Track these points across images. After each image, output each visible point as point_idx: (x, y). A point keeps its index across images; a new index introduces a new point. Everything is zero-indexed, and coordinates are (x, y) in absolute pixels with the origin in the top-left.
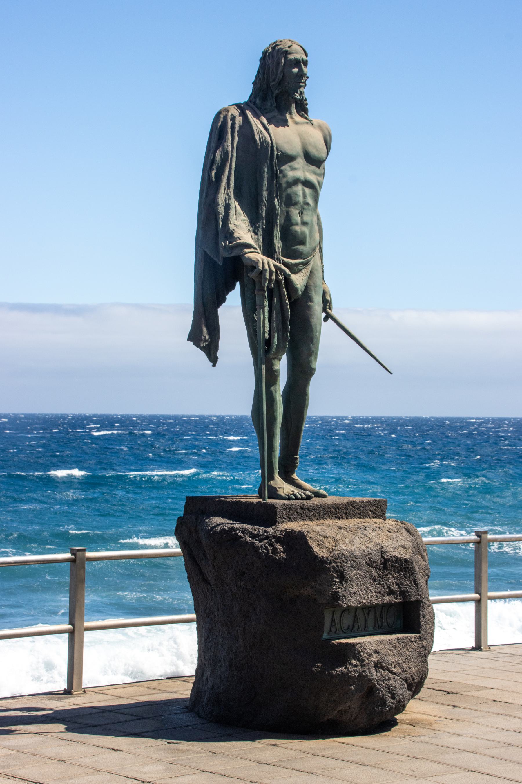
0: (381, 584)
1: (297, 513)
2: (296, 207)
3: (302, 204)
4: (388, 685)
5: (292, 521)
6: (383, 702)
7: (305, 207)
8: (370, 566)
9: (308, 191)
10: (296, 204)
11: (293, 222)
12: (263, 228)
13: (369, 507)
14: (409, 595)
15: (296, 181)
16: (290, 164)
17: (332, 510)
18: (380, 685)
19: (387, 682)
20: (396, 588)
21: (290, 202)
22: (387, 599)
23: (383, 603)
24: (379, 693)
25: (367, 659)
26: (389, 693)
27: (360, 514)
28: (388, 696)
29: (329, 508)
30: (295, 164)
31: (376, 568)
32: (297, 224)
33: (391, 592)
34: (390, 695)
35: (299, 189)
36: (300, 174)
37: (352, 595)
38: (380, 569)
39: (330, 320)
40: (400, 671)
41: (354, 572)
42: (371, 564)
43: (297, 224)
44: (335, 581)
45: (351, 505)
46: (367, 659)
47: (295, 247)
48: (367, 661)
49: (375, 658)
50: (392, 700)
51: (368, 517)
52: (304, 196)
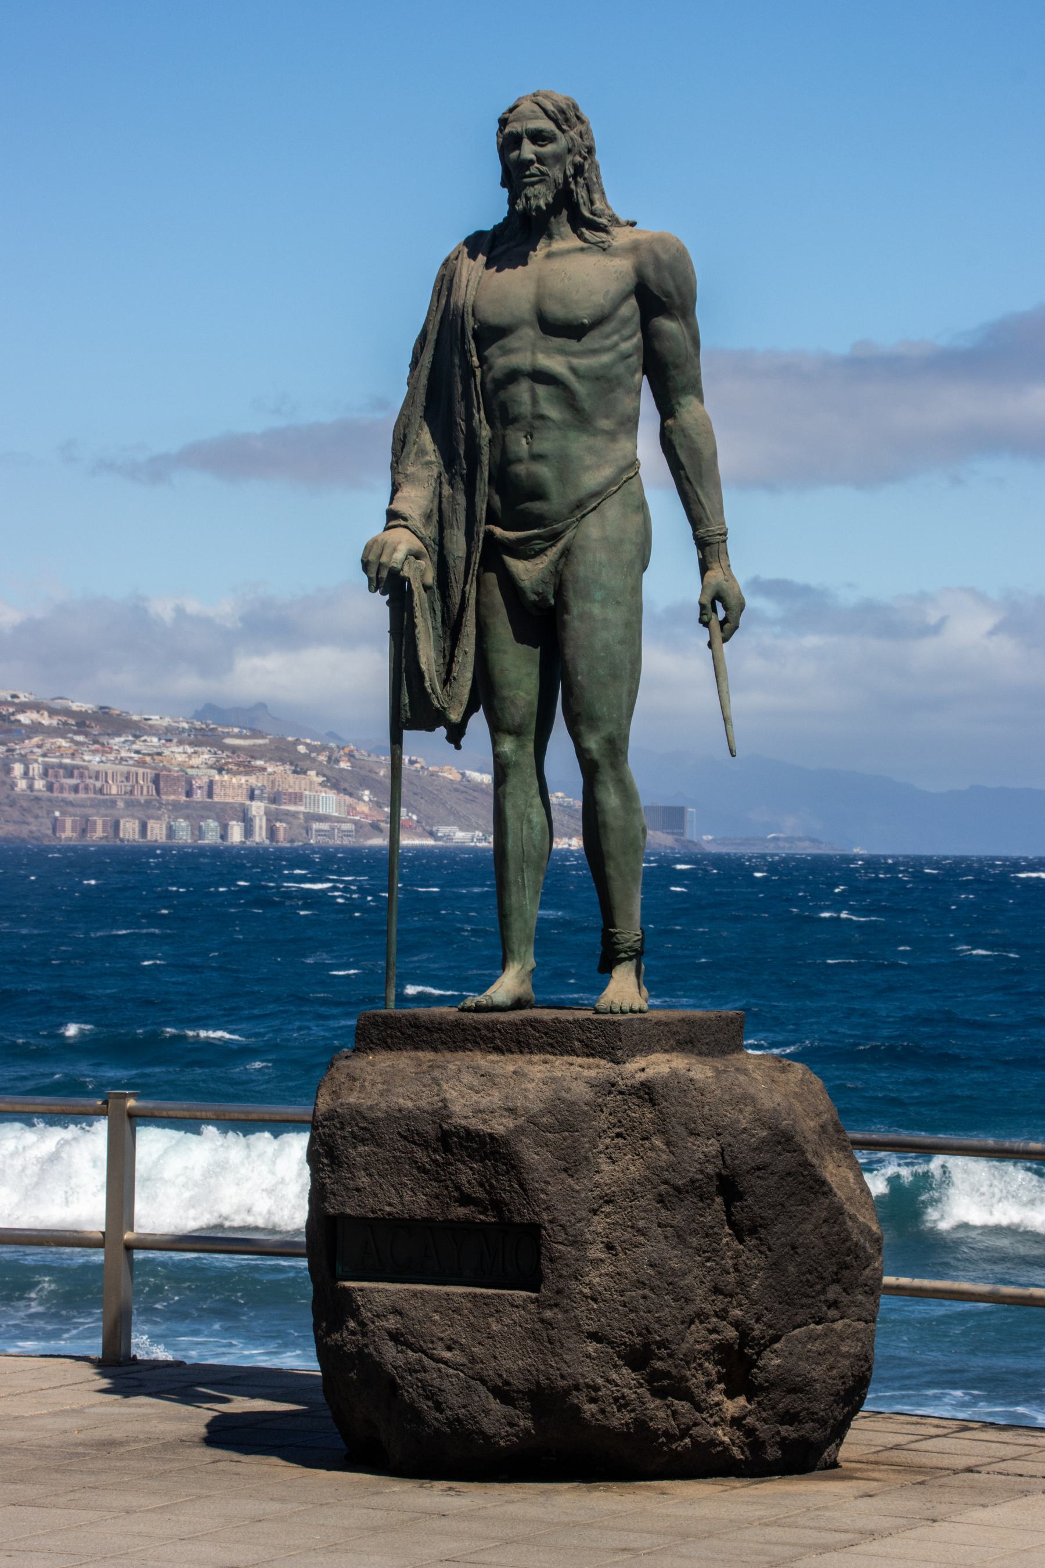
0: (441, 1181)
1: (402, 1034)
2: (517, 425)
3: (529, 419)
4: (421, 1381)
5: (391, 1050)
6: (418, 1415)
7: (537, 423)
8: (409, 1142)
9: (541, 390)
10: (515, 420)
11: (512, 456)
12: (462, 476)
13: (576, 1032)
14: (509, 1210)
15: (513, 376)
16: (500, 343)
17: (484, 1032)
18: (402, 1378)
19: (419, 1376)
20: (480, 1193)
21: (502, 417)
22: (461, 1212)
23: (446, 1221)
24: (402, 1395)
25: (373, 1322)
26: (427, 1398)
27: (552, 1046)
28: (425, 1405)
29: (476, 1028)
30: (511, 341)
31: (425, 1145)
32: (519, 460)
33: (465, 1200)
34: (430, 1404)
35: (522, 391)
36: (522, 360)
37: (350, 1194)
38: (435, 1151)
40: (465, 1360)
41: (361, 1149)
42: (413, 1137)
43: (519, 460)
44: (323, 1163)
45: (531, 1026)
46: (373, 1322)
47: (522, 506)
48: (373, 1327)
49: (392, 1322)
50: (438, 1415)
51: (574, 1052)
52: (535, 401)
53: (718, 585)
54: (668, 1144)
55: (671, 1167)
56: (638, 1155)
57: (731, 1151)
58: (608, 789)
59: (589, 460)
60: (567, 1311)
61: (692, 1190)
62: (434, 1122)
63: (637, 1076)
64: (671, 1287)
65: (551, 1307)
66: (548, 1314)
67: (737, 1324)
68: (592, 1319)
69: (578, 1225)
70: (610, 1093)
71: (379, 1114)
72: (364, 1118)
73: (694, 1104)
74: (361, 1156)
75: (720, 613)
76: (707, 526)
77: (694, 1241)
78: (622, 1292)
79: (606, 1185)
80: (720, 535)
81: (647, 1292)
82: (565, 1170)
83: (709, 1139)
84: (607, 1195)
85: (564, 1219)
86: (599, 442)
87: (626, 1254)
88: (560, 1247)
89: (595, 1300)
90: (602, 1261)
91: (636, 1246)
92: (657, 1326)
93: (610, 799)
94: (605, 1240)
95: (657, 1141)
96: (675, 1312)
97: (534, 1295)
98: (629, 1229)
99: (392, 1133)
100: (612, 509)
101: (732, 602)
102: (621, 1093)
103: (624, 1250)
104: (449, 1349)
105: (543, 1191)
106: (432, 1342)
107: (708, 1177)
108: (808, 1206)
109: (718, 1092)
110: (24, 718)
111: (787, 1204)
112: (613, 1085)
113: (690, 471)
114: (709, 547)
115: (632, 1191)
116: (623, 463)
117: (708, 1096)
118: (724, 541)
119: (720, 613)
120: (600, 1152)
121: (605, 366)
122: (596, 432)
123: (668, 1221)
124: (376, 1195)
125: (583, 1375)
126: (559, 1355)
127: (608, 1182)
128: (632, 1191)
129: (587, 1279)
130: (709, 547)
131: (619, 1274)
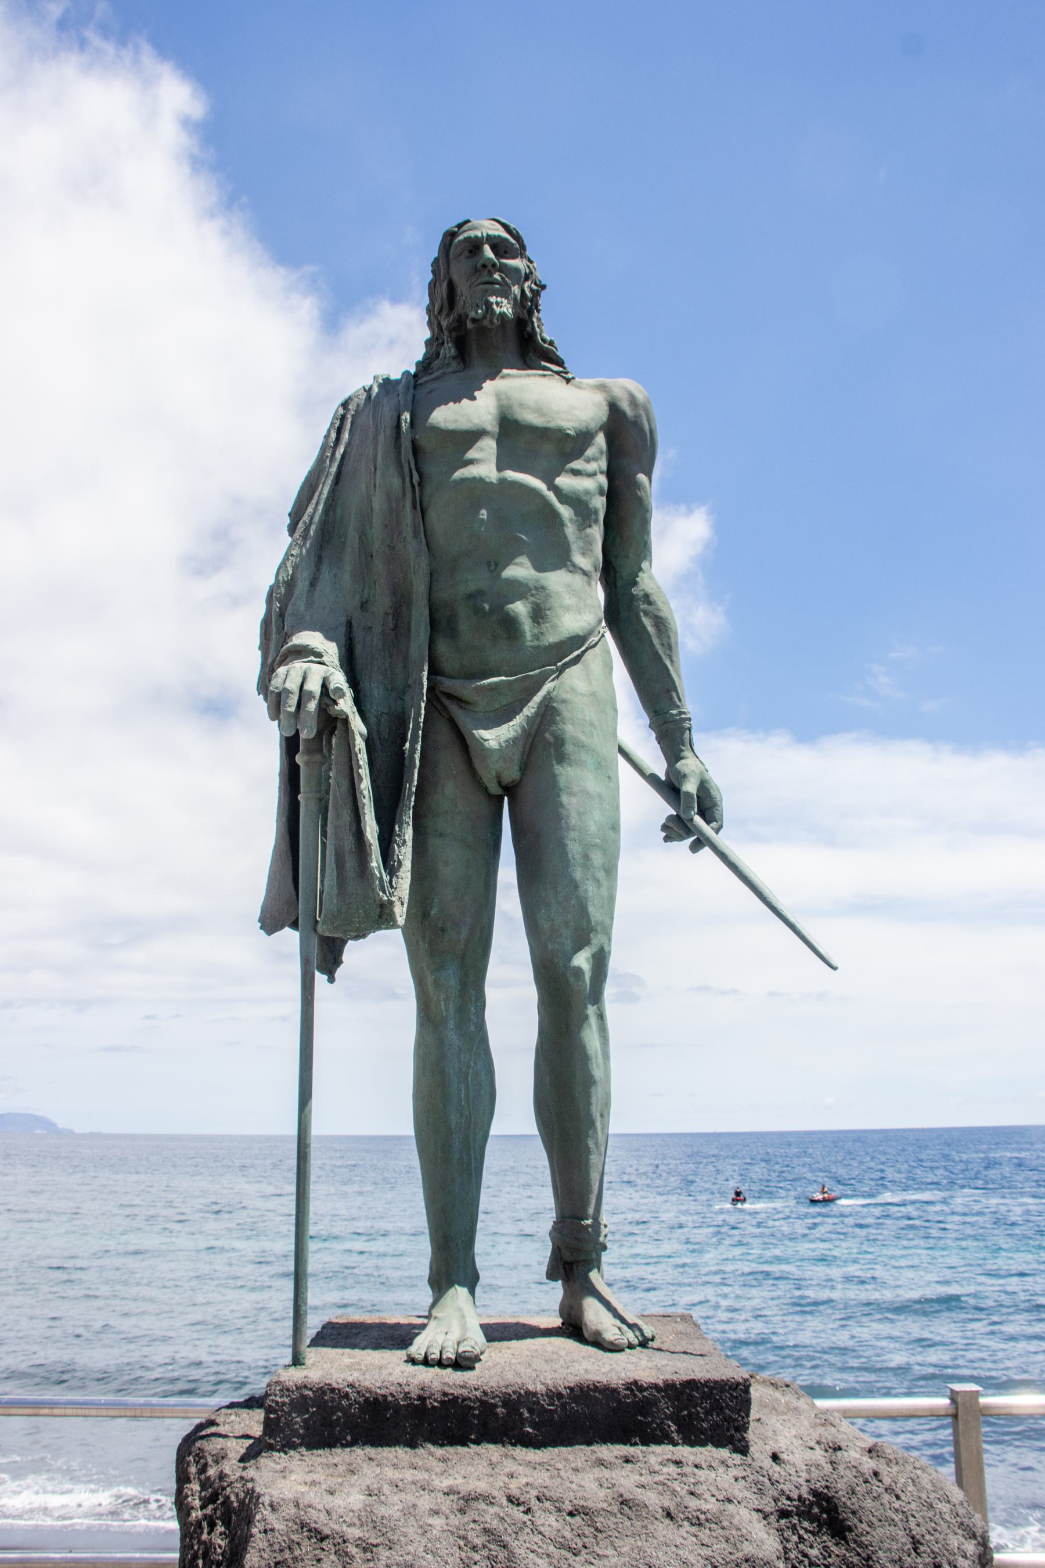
39: (707, 849)
59: (568, 600)
122: (575, 569)
130: (672, 733)
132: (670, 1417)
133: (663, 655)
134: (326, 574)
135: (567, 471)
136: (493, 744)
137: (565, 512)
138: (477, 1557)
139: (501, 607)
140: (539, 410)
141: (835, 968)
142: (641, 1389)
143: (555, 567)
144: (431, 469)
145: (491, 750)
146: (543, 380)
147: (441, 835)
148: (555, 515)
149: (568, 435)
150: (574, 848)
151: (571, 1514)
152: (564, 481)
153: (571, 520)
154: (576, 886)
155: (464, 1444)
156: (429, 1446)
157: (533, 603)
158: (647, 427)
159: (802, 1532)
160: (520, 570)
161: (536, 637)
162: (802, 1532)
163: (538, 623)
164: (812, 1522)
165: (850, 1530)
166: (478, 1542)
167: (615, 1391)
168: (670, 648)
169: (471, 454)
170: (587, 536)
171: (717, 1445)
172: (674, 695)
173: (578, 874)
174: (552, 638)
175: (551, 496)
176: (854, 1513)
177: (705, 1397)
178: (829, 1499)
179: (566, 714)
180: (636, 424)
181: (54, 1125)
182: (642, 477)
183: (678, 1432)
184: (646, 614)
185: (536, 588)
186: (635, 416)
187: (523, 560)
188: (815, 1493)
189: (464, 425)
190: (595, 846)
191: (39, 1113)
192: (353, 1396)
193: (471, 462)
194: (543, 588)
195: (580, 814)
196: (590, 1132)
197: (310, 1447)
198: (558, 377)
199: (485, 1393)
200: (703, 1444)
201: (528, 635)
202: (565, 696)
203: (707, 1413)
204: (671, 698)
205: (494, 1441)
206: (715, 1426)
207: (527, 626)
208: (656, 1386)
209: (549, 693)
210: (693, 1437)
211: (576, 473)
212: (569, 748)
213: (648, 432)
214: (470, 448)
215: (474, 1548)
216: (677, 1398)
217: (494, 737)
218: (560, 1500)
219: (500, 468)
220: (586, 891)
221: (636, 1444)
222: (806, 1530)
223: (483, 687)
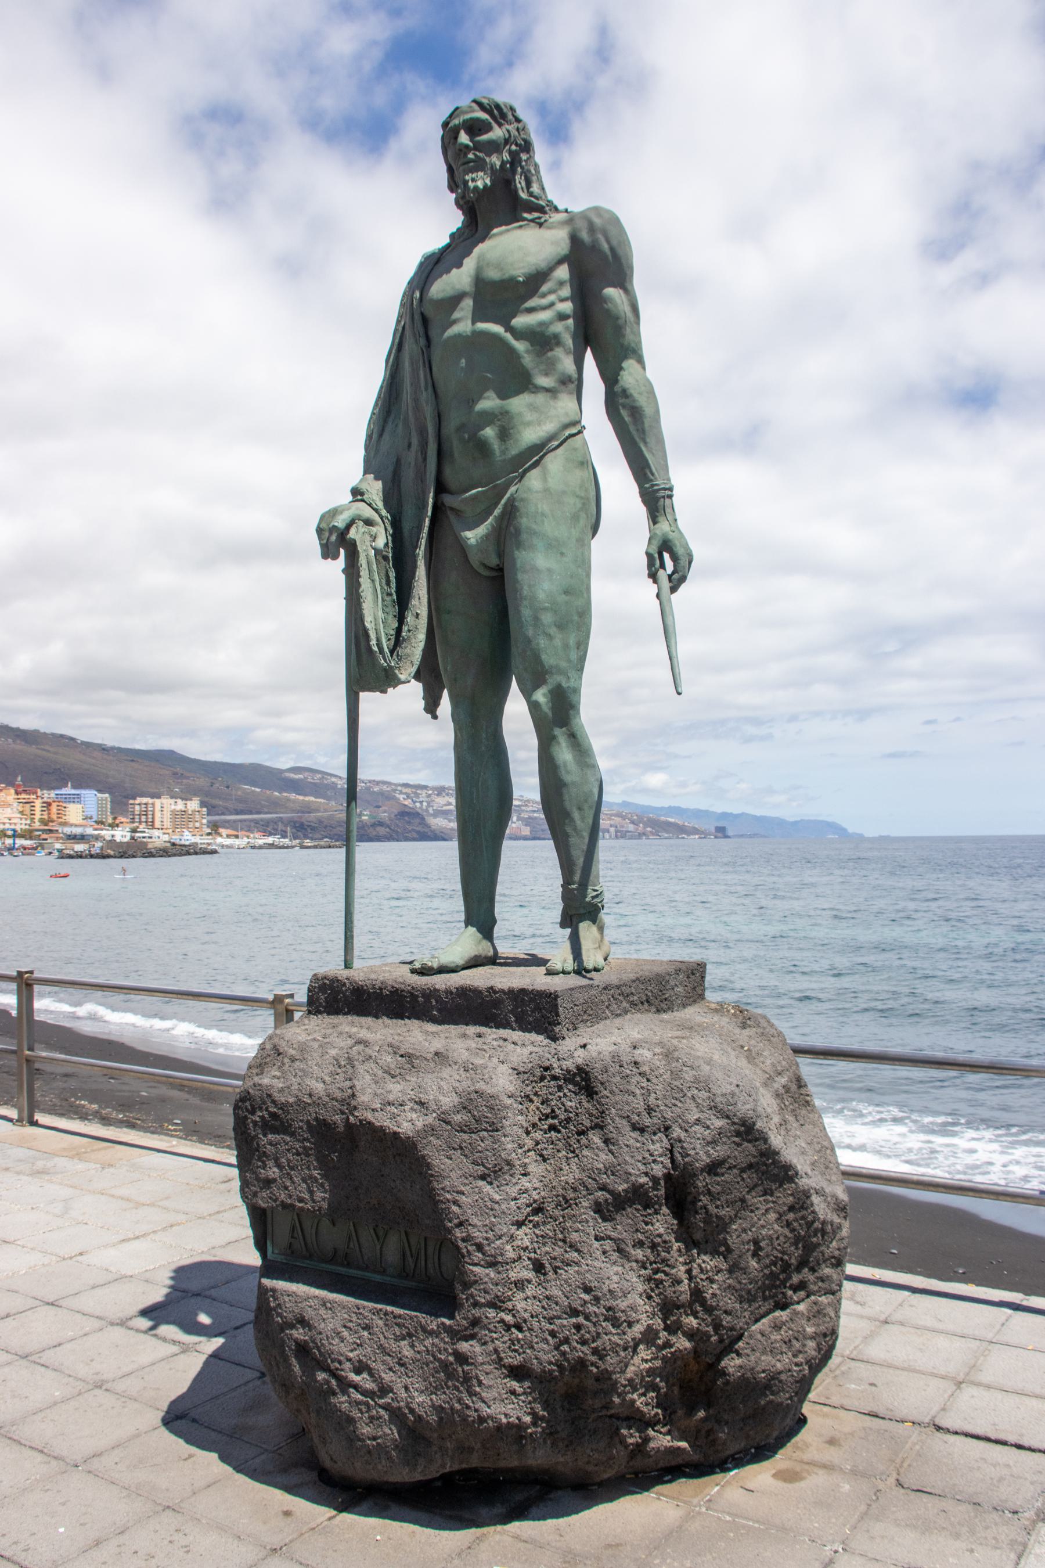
42: (322, 1130)
53: (664, 535)
54: (607, 1141)
55: (611, 1170)
56: (573, 1152)
57: (682, 1147)
58: (559, 743)
59: (529, 416)
60: (485, 1343)
61: (637, 1197)
62: (343, 1113)
63: (576, 1054)
64: (610, 1313)
65: (466, 1338)
66: (464, 1346)
67: (691, 1335)
68: (516, 1351)
69: (498, 1242)
70: (542, 1078)
71: (291, 1100)
72: (274, 1102)
73: (638, 1092)
74: (271, 1144)
75: (668, 562)
76: (652, 481)
77: (639, 1254)
78: (550, 1320)
79: (535, 1189)
80: (665, 489)
81: (581, 1319)
82: (483, 1177)
83: (655, 1134)
84: (535, 1201)
85: (478, 1235)
86: (540, 398)
87: (556, 1273)
88: (476, 1269)
89: (519, 1328)
90: (529, 1281)
91: (568, 1265)
92: (593, 1358)
93: (564, 754)
94: (532, 1255)
95: (596, 1138)
96: (615, 1339)
97: (447, 1322)
98: (560, 1243)
99: (302, 1121)
100: (555, 463)
101: (680, 551)
102: (555, 1078)
103: (555, 1270)
104: (358, 1372)
105: (456, 1203)
106: (340, 1362)
107: (655, 1180)
108: (772, 1195)
109: (667, 1076)
110: (516, 713)
111: (748, 1197)
112: (546, 1069)
113: (633, 423)
114: (656, 500)
115: (564, 1197)
116: (566, 420)
117: (654, 1081)
118: (670, 497)
119: (668, 562)
120: (529, 1150)
121: (542, 324)
122: (537, 389)
123: (608, 1233)
124: (286, 1188)
125: (506, 1415)
126: (476, 1394)
127: (537, 1185)
128: (564, 1197)
129: (509, 1305)
130: (656, 500)
131: (548, 1298)
132: (511, 1012)
133: (638, 439)
134: (389, 427)
135: (522, 312)
136: (473, 541)
137: (520, 346)
138: (339, 1071)
139: (475, 434)
140: (498, 266)
141: (679, 694)
142: (495, 992)
143: (518, 393)
144: (433, 333)
145: (472, 546)
146: (519, 232)
147: (449, 612)
148: (512, 350)
149: (518, 282)
150: (526, 613)
151: (402, 1056)
152: (520, 321)
153: (527, 352)
154: (530, 641)
155: (402, 1019)
156: (385, 1018)
157: (500, 426)
158: (605, 246)
159: (566, 1091)
160: (489, 402)
161: (503, 452)
162: (566, 1091)
163: (505, 441)
164: (575, 1086)
165: (597, 1094)
166: (343, 1063)
167: (480, 992)
168: (644, 431)
169: (456, 315)
170: (549, 358)
171: (538, 1033)
172: (648, 472)
173: (530, 633)
174: (514, 452)
175: (508, 336)
176: (602, 1084)
177: (531, 1000)
178: (587, 1073)
179: (523, 510)
180: (595, 248)
181: (844, 830)
182: (612, 292)
183: (516, 1021)
184: (624, 407)
185: (501, 414)
186: (593, 241)
187: (491, 394)
188: (578, 1068)
189: (449, 292)
190: (545, 609)
191: (829, 819)
192: (348, 985)
193: (454, 322)
194: (507, 412)
195: (530, 586)
196: (567, 821)
197: (329, 1014)
198: (532, 224)
199: (413, 988)
200: (530, 1032)
201: (497, 453)
202: (524, 496)
203: (533, 1011)
204: (645, 474)
205: (418, 1018)
206: (536, 1020)
207: (496, 445)
208: (503, 991)
209: (512, 495)
210: (525, 1027)
211: (531, 310)
212: (524, 536)
213: (608, 253)
214: (454, 310)
215: (340, 1067)
216: (515, 1000)
217: (472, 536)
218: (399, 1048)
219: (473, 323)
220: (538, 644)
221: (491, 1027)
222: (570, 1091)
223: (466, 498)
